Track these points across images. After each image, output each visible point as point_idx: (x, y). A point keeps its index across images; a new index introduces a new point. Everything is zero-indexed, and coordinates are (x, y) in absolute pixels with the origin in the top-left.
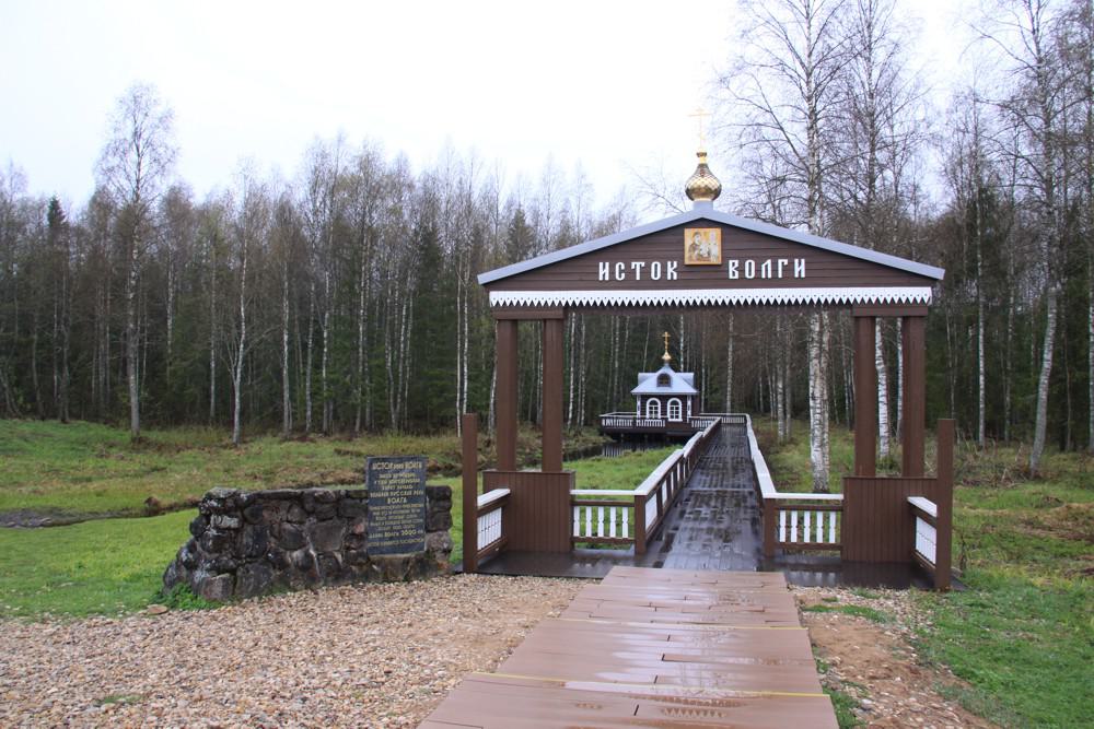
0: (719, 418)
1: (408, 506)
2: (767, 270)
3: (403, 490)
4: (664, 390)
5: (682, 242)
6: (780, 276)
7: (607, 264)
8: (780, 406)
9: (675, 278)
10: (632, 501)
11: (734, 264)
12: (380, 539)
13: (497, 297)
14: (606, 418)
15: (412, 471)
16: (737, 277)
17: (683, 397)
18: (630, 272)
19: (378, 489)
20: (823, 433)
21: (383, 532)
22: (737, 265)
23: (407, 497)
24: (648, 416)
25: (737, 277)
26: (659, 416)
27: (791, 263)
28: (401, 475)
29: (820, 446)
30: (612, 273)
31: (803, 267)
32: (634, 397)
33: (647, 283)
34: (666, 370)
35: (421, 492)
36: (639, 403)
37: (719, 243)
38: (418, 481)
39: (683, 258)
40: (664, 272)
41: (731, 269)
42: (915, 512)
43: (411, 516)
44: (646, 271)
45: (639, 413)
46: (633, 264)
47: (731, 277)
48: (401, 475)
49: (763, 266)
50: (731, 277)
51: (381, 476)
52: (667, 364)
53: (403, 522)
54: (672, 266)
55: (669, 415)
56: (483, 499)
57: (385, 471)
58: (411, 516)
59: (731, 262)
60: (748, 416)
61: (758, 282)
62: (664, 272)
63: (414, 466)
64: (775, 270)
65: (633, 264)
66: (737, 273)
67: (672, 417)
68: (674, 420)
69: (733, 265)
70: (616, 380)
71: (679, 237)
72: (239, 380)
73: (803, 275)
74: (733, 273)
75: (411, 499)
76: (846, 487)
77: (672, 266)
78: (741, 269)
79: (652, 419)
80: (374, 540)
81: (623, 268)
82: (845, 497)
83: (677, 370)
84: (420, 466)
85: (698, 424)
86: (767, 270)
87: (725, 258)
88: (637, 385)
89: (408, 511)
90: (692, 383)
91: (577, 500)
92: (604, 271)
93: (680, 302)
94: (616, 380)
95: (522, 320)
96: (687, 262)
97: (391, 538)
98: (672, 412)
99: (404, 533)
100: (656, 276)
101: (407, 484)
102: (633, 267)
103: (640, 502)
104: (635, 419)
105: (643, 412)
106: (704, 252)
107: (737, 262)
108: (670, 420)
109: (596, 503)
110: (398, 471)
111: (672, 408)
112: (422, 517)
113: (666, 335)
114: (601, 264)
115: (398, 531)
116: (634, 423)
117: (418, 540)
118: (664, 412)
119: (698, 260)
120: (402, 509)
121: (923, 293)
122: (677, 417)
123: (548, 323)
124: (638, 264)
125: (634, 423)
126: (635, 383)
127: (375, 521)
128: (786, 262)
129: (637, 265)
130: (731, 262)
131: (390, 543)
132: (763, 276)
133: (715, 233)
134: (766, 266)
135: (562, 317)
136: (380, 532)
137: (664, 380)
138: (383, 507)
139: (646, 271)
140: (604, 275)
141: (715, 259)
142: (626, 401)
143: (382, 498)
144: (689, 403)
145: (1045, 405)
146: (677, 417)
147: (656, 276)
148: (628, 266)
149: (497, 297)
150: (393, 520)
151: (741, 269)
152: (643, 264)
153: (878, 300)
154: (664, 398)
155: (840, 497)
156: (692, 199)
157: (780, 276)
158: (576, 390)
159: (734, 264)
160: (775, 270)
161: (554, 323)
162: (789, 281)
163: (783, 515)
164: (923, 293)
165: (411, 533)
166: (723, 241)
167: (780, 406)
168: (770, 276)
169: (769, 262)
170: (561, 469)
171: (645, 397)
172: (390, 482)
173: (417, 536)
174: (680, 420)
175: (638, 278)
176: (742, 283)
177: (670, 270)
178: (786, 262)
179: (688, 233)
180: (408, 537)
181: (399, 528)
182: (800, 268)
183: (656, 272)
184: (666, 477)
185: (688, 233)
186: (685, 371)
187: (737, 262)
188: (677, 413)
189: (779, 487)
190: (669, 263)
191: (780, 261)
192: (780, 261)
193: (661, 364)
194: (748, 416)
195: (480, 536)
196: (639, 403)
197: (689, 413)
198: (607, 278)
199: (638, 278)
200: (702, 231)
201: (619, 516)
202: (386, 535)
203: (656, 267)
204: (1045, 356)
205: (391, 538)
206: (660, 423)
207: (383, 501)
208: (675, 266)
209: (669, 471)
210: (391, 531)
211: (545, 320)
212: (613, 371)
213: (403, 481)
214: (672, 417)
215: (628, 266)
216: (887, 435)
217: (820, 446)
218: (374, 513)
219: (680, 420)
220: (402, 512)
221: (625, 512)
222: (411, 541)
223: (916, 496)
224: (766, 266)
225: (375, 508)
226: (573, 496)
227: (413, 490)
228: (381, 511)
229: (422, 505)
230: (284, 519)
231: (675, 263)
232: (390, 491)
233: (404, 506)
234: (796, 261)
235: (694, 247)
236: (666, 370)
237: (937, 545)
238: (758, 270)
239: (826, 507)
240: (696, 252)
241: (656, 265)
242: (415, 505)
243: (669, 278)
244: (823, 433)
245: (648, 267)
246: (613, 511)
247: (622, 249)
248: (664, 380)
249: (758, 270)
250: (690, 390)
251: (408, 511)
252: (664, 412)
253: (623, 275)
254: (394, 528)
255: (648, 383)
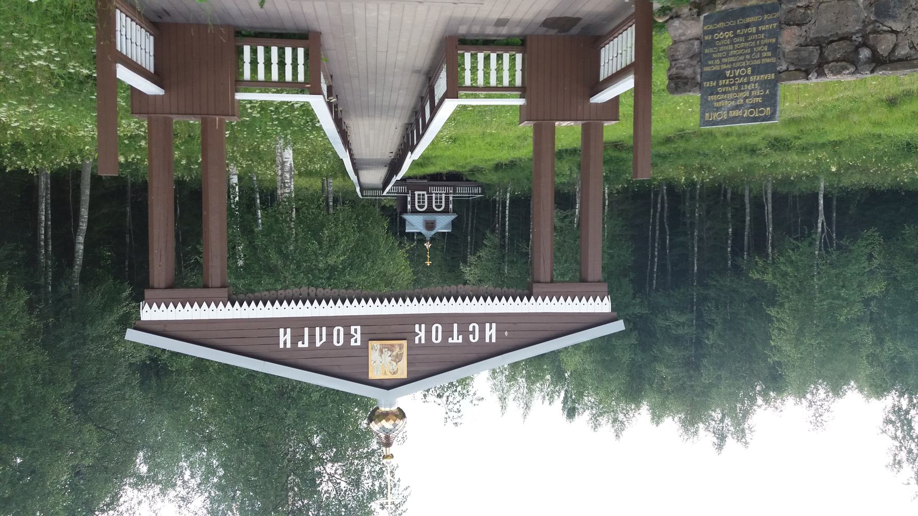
0: (384, 194)
1: (724, 67)
2: (321, 335)
3: (730, 86)
4: (430, 217)
5: (409, 364)
6: (306, 330)
7: (487, 340)
8: (331, 204)
9: (417, 326)
10: (461, 93)
11: (356, 341)
12: (762, 23)
13: (603, 306)
14: (479, 194)
15: (718, 109)
16: (353, 328)
17: (414, 211)
18: (464, 331)
19: (764, 84)
20: (282, 175)
21: (758, 32)
22: (353, 340)
23: (726, 78)
24: (443, 196)
25: (353, 328)
26: (434, 195)
27: (294, 343)
28: (733, 103)
29: (284, 162)
30: (482, 331)
31: (494, 331)
32: (454, 211)
33: (446, 320)
34: (429, 234)
35: (706, 84)
36: (451, 206)
37: (371, 363)
38: (710, 98)
39: (409, 348)
40: (428, 332)
41: (358, 336)
42: (155, 77)
43: (720, 55)
44: (448, 333)
45: (451, 199)
46: (460, 341)
47: (359, 328)
48: (733, 103)
49: (324, 339)
50: (359, 328)
51: (759, 100)
52: (428, 239)
53: (731, 47)
54: (420, 339)
55: (426, 196)
56: (627, 84)
57: (754, 106)
58: (720, 55)
59: (359, 343)
60: (360, 196)
61: (330, 323)
62: (428, 332)
63: (716, 115)
64: (312, 336)
65: (460, 341)
66: (352, 332)
67: (423, 195)
68: (421, 193)
69: (357, 340)
70: (470, 226)
71: (413, 369)
72: (820, 221)
73: (282, 331)
74: (357, 331)
75: (720, 75)
76: (233, 107)
77: (420, 339)
78: (348, 336)
79: (441, 194)
80: (770, 22)
81: (471, 336)
82: (233, 96)
83: (420, 234)
84: (707, 115)
85: (402, 189)
86: (321, 335)
87: (364, 348)
88: (453, 222)
89: (724, 60)
90: (407, 223)
91: (519, 93)
92: (491, 333)
93: (412, 301)
94: (470, 226)
95: (599, 282)
96: (405, 343)
97: (747, 26)
98: (424, 199)
99: (730, 34)
100: (437, 328)
101: (725, 93)
102: (461, 337)
103: (451, 93)
104: (454, 193)
105: (447, 199)
106: (387, 353)
107: (353, 343)
108: (425, 193)
109: (500, 90)
110: (737, 107)
111: (441, 202)
112: (706, 55)
113: (428, 263)
114: (494, 340)
115: (737, 36)
116: (455, 190)
117: (711, 27)
118: (430, 199)
119: (393, 346)
120: (732, 63)
121: (149, 313)
122: (419, 195)
123: (548, 279)
124: (455, 341)
125: (455, 190)
126: (454, 223)
127: (769, 45)
128: (300, 345)
129: (457, 339)
130: (359, 343)
131: (749, 20)
132: (324, 329)
133: (373, 375)
134: (321, 340)
135: (534, 285)
136: (762, 32)
137: (430, 225)
138: (758, 62)
139: (448, 333)
140: (491, 329)
141: (375, 345)
142: (460, 205)
143: (759, 73)
144: (409, 207)
145: (82, 202)
146: (419, 195)
147: (437, 328)
148: (466, 339)
149: (603, 306)
150: (745, 48)
151: (348, 336)
152: (450, 340)
153: (200, 306)
154: (430, 211)
155: (239, 96)
156: (399, 408)
157: (306, 330)
158: (504, 217)
159: (356, 341)
160: (312, 336)
161: (542, 280)
162: (297, 325)
163: (301, 78)
164: (149, 313)
165: (721, 35)
166: (367, 366)
167: (331, 204)
168: (318, 329)
169: (318, 344)
170: (534, 124)
171: (446, 211)
172: (747, 94)
173: (712, 32)
174: (416, 193)
175: (455, 325)
176: (347, 322)
177: (422, 334)
178: (300, 345)
179: (403, 374)
180: (725, 30)
181: (736, 40)
182: (285, 338)
183: (437, 332)
184: (426, 127)
185: (402, 373)
186: (413, 233)
187: (353, 343)
188: (419, 199)
189: (307, 110)
190: (423, 341)
191: (306, 345)
192: (306, 345)
193: (432, 240)
194: (360, 196)
195: (602, 68)
196: (451, 206)
197: (409, 199)
198: (488, 325)
199: (455, 325)
200: (389, 376)
201: (254, 70)
202: (754, 30)
203: (437, 338)
204: (82, 247)
205: (747, 26)
206: (434, 191)
207: (756, 70)
208: (417, 339)
209: (423, 134)
210: (746, 35)
211: (552, 281)
212: (472, 232)
213: (731, 96)
214: (423, 195)
215: (466, 339)
216: (231, 177)
217: (284, 162)
218: (769, 54)
219: (416, 193)
220: (732, 59)
221: (468, 82)
222: (721, 25)
223: (155, 96)
224: (321, 340)
225: (768, 60)
226: (521, 97)
227: (718, 86)
228: (761, 58)
229: (707, 69)
230: (901, 37)
231: (417, 342)
232: (748, 83)
233: (729, 66)
234: (289, 346)
235: (398, 358)
236: (429, 234)
237: (155, 56)
238: (330, 335)
239: (254, 85)
240: (394, 353)
241: (437, 339)
242: (717, 68)
243: (423, 326)
244: (282, 175)
245: (445, 338)
246: (481, 82)
247: (473, 356)
248: (430, 225)
249: (330, 335)
250: (408, 217)
251: (724, 60)
252: (430, 199)
253: (471, 329)
254: (742, 39)
255: (443, 223)
